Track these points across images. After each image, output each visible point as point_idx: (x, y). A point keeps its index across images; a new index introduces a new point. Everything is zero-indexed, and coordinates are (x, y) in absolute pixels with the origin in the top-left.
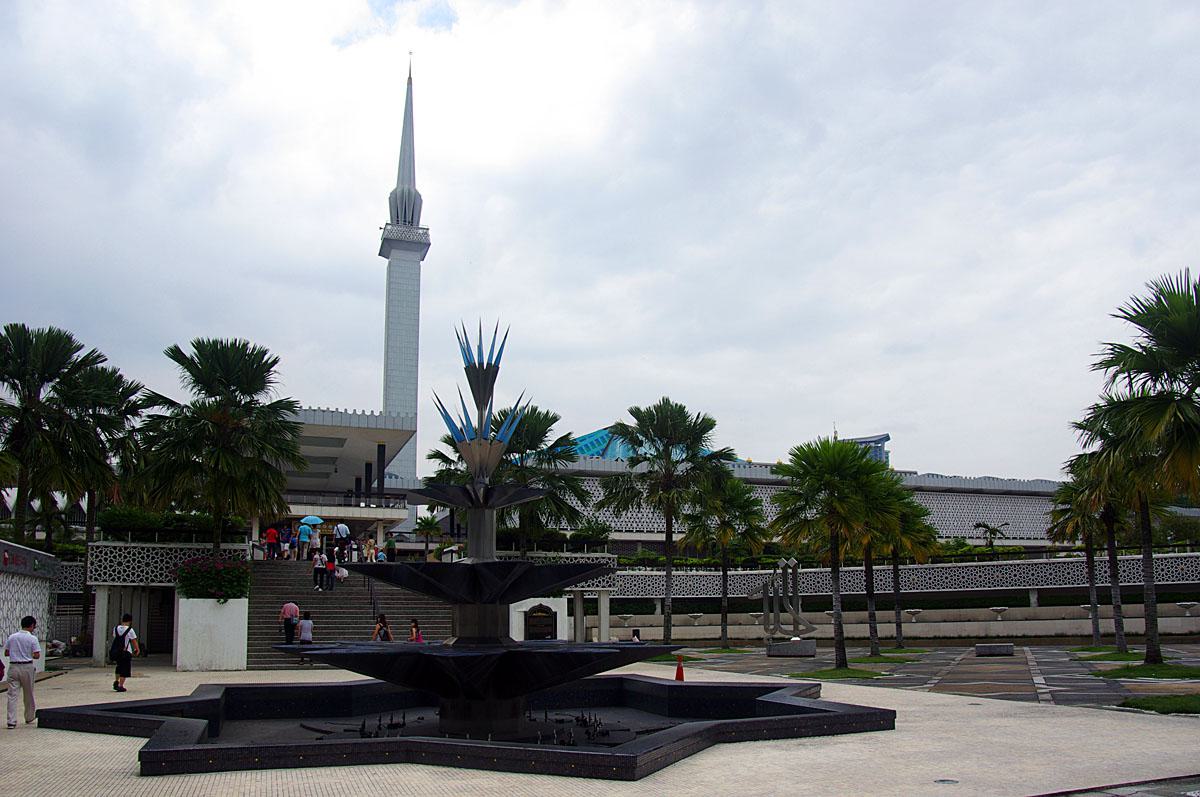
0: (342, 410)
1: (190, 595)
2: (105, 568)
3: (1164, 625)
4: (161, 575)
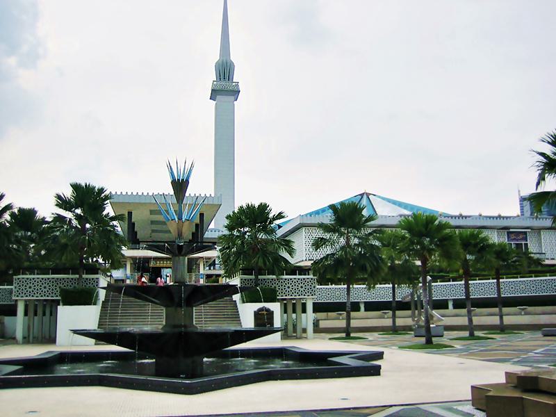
1: (65, 304)
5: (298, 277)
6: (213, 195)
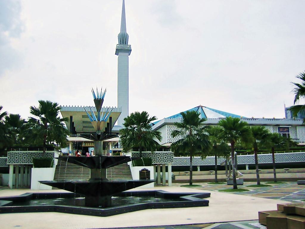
0: (77, 106)
1: (35, 167)
2: (21, 159)
3: (261, 176)
4: (29, 161)
5: (163, 152)
6: (117, 107)
